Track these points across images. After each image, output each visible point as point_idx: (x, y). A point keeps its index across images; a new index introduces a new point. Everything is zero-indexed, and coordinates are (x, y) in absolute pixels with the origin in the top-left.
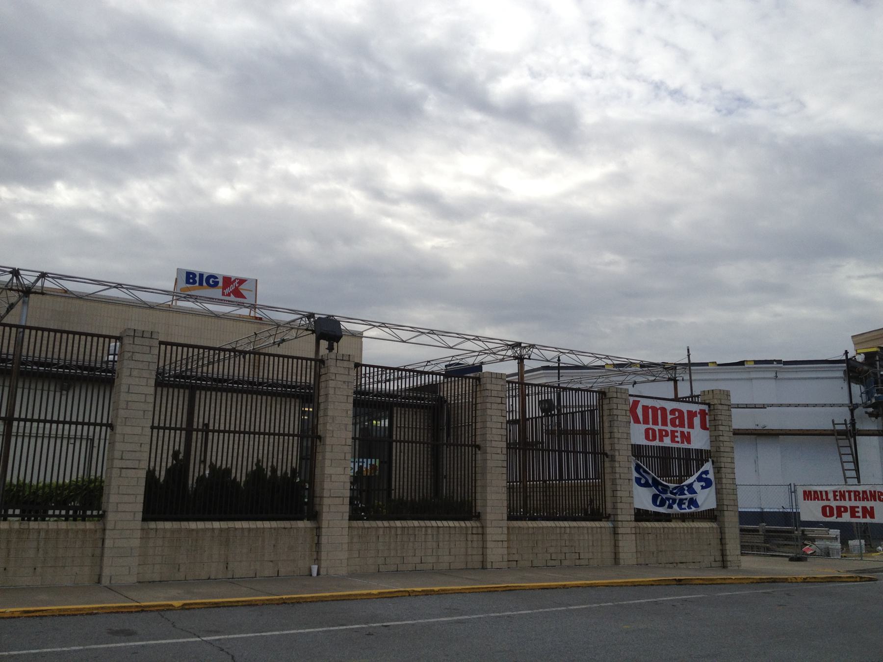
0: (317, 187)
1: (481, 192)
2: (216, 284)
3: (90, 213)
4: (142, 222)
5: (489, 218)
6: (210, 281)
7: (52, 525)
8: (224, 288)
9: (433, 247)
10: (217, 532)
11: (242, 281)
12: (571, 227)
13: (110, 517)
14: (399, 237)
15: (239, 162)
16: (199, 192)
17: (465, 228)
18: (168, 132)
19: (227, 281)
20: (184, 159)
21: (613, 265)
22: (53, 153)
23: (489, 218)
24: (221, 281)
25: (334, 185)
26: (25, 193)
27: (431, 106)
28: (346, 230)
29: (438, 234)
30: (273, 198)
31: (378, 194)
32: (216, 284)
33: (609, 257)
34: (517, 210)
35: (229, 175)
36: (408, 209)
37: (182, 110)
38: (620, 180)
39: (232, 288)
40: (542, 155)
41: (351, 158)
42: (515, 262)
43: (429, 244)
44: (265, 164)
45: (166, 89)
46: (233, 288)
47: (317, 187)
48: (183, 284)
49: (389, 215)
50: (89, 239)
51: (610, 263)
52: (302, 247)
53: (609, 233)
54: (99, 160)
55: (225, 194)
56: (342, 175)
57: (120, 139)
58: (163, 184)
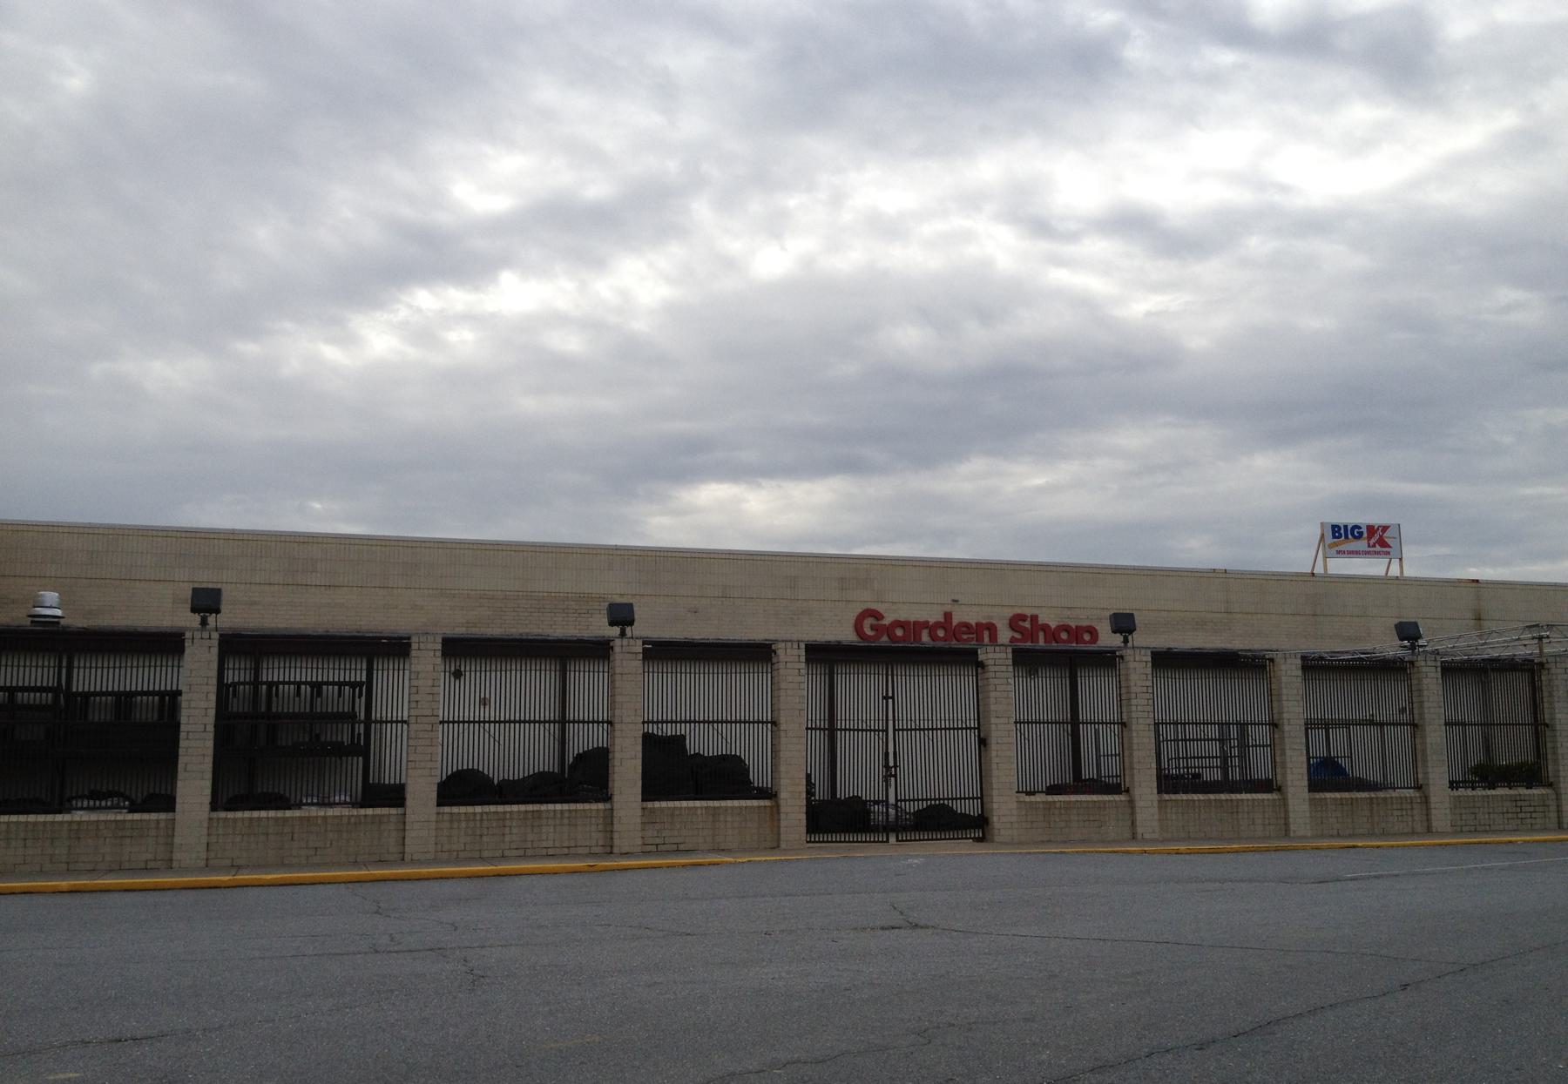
0: (928, 229)
1: (1241, 197)
2: (1360, 535)
3: (559, 320)
4: (640, 326)
5: (1257, 245)
6: (1354, 532)
7: (79, 816)
8: (1369, 538)
9: (1149, 314)
10: (345, 820)
11: (1385, 528)
12: (1424, 244)
13: (616, 798)
14: (1084, 303)
15: (792, 202)
16: (730, 264)
17: (1210, 270)
18: (672, 166)
19: (1371, 530)
20: (701, 210)
21: (1517, 309)
22: (496, 226)
23: (1257, 245)
24: (1364, 530)
25: (958, 222)
26: (457, 298)
27: (1137, 52)
28: (981, 299)
29: (1156, 288)
30: (851, 259)
31: (1041, 227)
32: (1360, 535)
33: (1507, 295)
34: (1315, 224)
35: (776, 226)
36: (1098, 247)
37: (692, 124)
38: (1528, 142)
39: (1377, 537)
40: (1361, 113)
41: (990, 167)
42: (1314, 323)
43: (1139, 308)
44: (837, 199)
45: (666, 91)
46: (1377, 538)
47: (928, 229)
48: (1329, 539)
49: (1059, 262)
50: (562, 363)
51: (1508, 308)
52: (909, 339)
53: (1499, 249)
54: (571, 228)
55: (772, 262)
56: (971, 201)
57: (597, 189)
58: (671, 255)
